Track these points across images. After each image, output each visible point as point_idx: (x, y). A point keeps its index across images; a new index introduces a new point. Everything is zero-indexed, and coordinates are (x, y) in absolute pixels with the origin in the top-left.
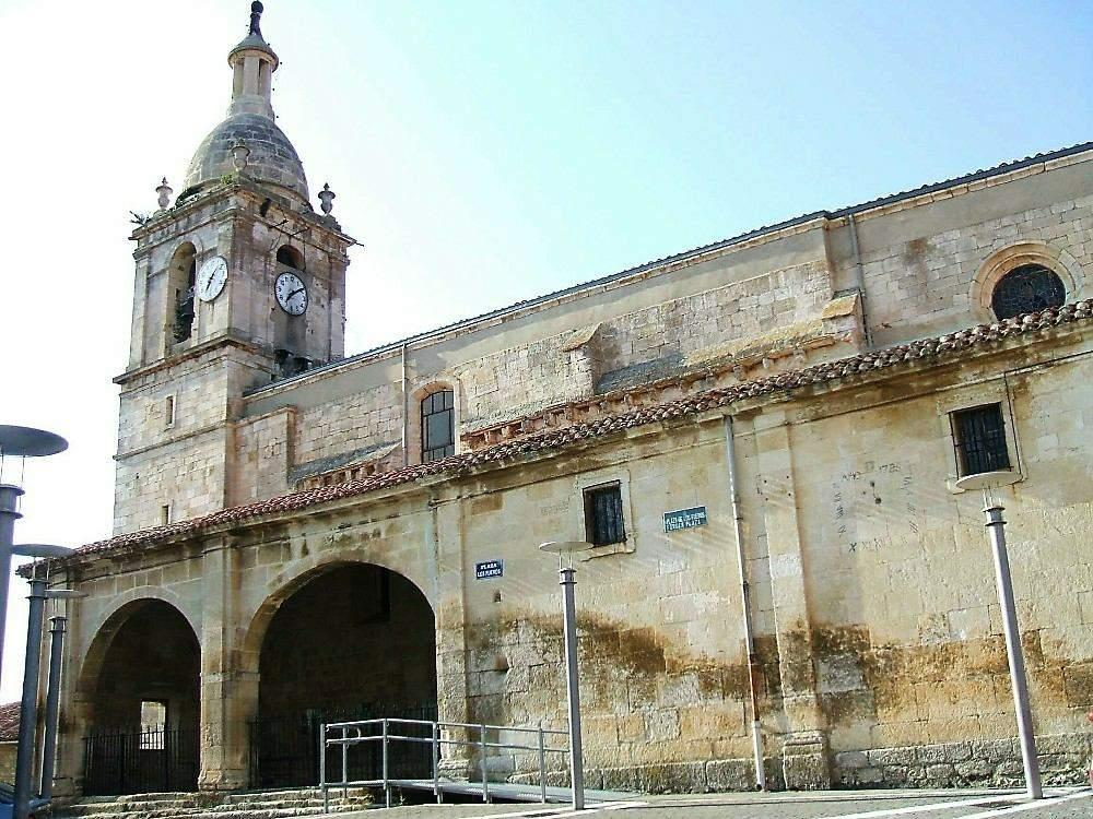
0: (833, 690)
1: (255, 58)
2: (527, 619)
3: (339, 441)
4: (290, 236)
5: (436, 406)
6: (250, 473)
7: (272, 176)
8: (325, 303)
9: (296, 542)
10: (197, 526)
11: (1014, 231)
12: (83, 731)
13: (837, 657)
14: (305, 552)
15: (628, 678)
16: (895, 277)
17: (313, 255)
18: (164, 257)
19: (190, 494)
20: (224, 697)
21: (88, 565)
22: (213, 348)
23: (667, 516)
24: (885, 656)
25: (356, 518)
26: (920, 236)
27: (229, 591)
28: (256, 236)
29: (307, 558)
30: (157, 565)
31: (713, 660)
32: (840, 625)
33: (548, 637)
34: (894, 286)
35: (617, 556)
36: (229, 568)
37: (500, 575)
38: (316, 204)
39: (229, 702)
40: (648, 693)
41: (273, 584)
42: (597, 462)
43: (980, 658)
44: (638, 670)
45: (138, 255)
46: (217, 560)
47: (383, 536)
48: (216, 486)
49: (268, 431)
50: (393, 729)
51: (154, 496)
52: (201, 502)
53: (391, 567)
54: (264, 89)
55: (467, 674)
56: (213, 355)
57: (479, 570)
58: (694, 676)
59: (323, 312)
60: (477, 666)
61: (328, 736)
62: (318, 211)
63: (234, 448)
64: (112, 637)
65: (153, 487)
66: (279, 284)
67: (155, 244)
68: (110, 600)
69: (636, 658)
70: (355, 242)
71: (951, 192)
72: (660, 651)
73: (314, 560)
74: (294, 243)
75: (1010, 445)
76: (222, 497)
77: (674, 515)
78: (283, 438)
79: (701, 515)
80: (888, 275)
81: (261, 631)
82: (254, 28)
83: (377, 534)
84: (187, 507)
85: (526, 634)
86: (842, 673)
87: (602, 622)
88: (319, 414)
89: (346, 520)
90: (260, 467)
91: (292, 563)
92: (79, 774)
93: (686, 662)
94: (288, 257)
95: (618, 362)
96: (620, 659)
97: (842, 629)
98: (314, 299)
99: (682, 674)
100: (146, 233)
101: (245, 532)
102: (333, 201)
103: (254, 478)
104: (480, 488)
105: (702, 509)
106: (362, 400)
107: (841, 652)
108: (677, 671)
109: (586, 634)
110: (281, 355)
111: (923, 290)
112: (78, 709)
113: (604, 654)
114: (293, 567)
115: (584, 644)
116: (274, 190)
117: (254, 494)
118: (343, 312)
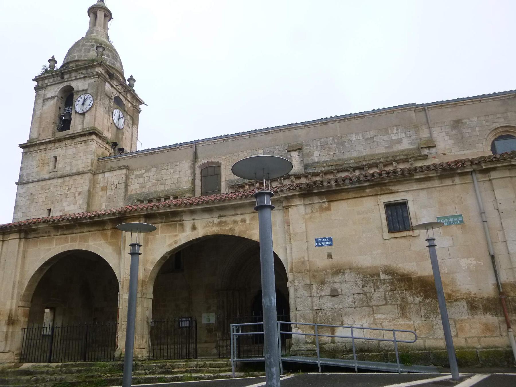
1: (99, 13)
2: (350, 269)
3: (155, 185)
4: (120, 93)
5: (210, 173)
6: (101, 197)
7: (112, 64)
8: (131, 126)
10: (56, 220)
12: (22, 324)
14: (194, 228)
15: (420, 302)
16: (447, 134)
18: (54, 91)
19: (65, 204)
21: (35, 230)
22: (84, 135)
26: (459, 118)
28: (107, 88)
29: (196, 232)
30: (86, 232)
31: (475, 294)
33: (365, 279)
34: (447, 138)
35: (408, 237)
37: (332, 245)
41: (171, 245)
42: (391, 190)
44: (426, 297)
45: (37, 89)
47: (248, 222)
48: (81, 201)
51: (41, 204)
56: (83, 139)
57: (317, 241)
58: (464, 303)
59: (130, 130)
60: (318, 293)
63: (93, 183)
64: (45, 271)
67: (48, 84)
68: (50, 249)
69: (425, 291)
71: (473, 101)
73: (200, 233)
74: (121, 97)
76: (86, 207)
78: (123, 181)
79: (459, 219)
80: (444, 134)
81: (158, 269)
83: (244, 221)
85: (349, 277)
87: (402, 271)
88: (143, 171)
89: (222, 213)
90: (108, 194)
91: (184, 234)
92: (17, 350)
93: (458, 294)
94: (118, 102)
95: (312, 159)
96: (414, 291)
99: (456, 300)
100: (42, 81)
103: (104, 199)
105: (461, 216)
106: (169, 167)
109: (390, 277)
110: (114, 145)
111: (461, 141)
112: (20, 311)
113: (402, 288)
115: (389, 283)
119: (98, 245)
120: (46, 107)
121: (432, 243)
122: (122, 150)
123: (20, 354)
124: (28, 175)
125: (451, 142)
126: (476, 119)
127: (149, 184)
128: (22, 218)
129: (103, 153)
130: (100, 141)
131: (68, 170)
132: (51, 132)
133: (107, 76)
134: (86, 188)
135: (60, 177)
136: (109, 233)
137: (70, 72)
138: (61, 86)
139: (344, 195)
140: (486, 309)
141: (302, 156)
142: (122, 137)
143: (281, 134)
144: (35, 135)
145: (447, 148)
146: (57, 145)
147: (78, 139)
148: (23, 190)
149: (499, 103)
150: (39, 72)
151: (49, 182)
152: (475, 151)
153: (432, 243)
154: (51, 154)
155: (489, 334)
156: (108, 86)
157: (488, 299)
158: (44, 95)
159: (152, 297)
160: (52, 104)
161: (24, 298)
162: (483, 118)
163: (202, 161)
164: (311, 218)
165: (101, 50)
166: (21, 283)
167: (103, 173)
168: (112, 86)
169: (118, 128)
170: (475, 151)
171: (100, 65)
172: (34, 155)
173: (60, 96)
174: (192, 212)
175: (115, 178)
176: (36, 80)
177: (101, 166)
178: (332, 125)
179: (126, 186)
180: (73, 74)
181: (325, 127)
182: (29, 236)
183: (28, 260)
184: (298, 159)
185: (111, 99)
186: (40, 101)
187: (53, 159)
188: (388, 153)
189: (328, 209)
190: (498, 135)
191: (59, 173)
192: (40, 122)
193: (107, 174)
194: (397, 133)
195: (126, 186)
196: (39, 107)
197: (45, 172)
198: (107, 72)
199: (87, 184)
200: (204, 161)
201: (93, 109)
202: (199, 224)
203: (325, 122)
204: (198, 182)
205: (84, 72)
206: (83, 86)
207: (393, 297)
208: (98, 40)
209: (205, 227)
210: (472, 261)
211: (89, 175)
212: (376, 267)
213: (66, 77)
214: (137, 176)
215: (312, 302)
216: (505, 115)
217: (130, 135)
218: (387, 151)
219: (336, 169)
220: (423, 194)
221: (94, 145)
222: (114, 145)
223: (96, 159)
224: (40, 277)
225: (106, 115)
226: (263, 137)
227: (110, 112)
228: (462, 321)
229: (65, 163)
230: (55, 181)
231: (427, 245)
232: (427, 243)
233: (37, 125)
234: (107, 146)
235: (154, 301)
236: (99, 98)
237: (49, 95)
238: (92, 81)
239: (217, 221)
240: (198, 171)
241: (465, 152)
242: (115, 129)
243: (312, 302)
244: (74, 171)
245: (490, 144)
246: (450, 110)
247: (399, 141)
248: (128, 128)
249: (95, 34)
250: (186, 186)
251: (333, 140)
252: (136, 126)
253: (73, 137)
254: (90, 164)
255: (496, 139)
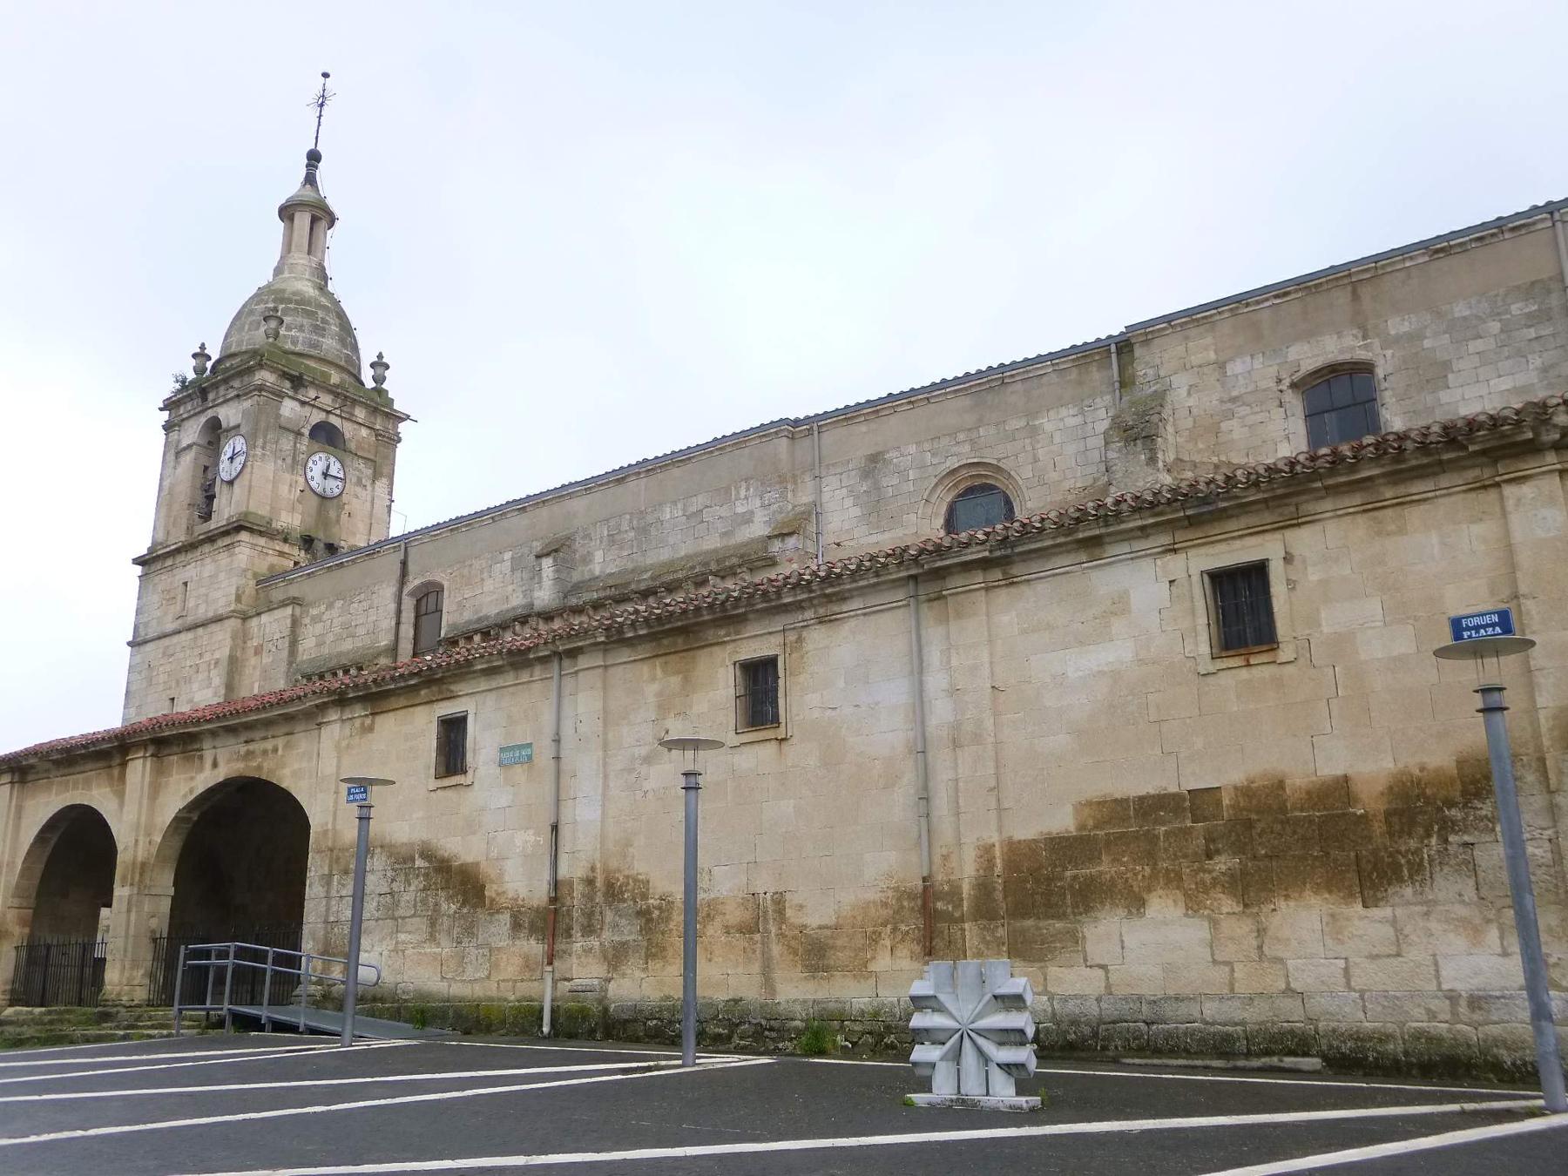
0: (616, 938)
1: (308, 215)
3: (340, 639)
4: (328, 412)
5: (428, 599)
6: (254, 668)
8: (368, 484)
9: (208, 756)
11: (967, 448)
13: (622, 906)
14: (215, 765)
17: (355, 433)
18: (192, 432)
19: (195, 686)
20: (129, 911)
21: (32, 767)
22: (226, 533)
23: (502, 750)
24: (660, 908)
25: (257, 735)
27: (145, 801)
29: (216, 772)
32: (626, 873)
34: (849, 502)
36: (147, 779)
38: (367, 376)
39: (133, 917)
40: (470, 931)
41: (185, 796)
43: (735, 915)
44: (464, 904)
45: (168, 427)
46: (139, 769)
48: (218, 679)
49: (273, 625)
50: (240, 953)
51: (161, 688)
52: (202, 694)
53: (283, 786)
54: (313, 245)
55: (328, 897)
56: (227, 540)
58: (505, 918)
61: (187, 957)
62: (369, 384)
63: (241, 638)
64: (53, 843)
65: (162, 678)
66: (310, 464)
69: (465, 893)
70: (408, 417)
72: (483, 887)
73: (221, 775)
75: (781, 702)
76: (223, 692)
77: (512, 748)
78: (287, 632)
81: (177, 843)
82: (310, 180)
83: (275, 750)
84: (191, 701)
86: (623, 922)
88: (323, 608)
94: (326, 436)
97: (627, 877)
98: (354, 480)
99: (498, 912)
101: (163, 740)
102: (387, 373)
104: (359, 711)
105: (530, 745)
107: (624, 901)
108: (494, 909)
110: (308, 542)
111: (875, 509)
114: (205, 778)
116: (312, 364)
117: (253, 685)
118: (390, 493)
119: (97, 795)
120: (179, 470)
121: (1494, 698)
122: (332, 549)
123: (13, 991)
124: (146, 624)
125: (857, 511)
126: (912, 449)
127: (330, 637)
128: (154, 709)
129: (272, 567)
130: (262, 541)
131: (203, 612)
132: (184, 526)
133: (288, 384)
134: (225, 652)
135: (189, 629)
136: (116, 772)
137: (215, 386)
138: (203, 419)
139: (394, 702)
140: (533, 930)
141: (563, 567)
142: (339, 516)
143: (544, 512)
144: (161, 537)
145: (848, 528)
146: (190, 556)
147: (220, 543)
148: (138, 658)
149: (966, 402)
150: (169, 388)
151: (175, 639)
152: (899, 532)
153: (1494, 698)
154: (181, 575)
155: (527, 975)
156: (289, 408)
157: (537, 910)
158: (179, 441)
159: (172, 891)
160: (188, 458)
161: (19, 892)
162: (927, 446)
163: (414, 582)
164: (348, 746)
165: (273, 324)
166: (11, 864)
167: (259, 614)
168: (303, 403)
169: (323, 498)
170: (899, 532)
171: (261, 366)
172: (157, 579)
173: (203, 442)
174: (214, 734)
175: (275, 625)
176: (169, 405)
177: (266, 592)
178: (632, 484)
179: (294, 643)
180: (222, 390)
181: (620, 489)
182: (30, 777)
183: (25, 822)
184: (551, 575)
185: (299, 434)
186: (171, 457)
187: (182, 588)
188: (727, 548)
189: (371, 729)
190: (962, 486)
191: (190, 620)
192: (170, 506)
193: (265, 618)
194: (746, 498)
195: (294, 643)
196: (169, 470)
197: (170, 617)
198: (285, 375)
199: (228, 642)
200: (417, 582)
201: (248, 470)
202: (223, 756)
203: (620, 477)
204: (407, 631)
205: (236, 383)
206: (281, 387)
207: (424, 902)
208: (284, 291)
209: (229, 761)
210: (530, 836)
211: (233, 623)
212: (412, 844)
213: (211, 396)
214: (317, 619)
215: (328, 910)
216: (974, 435)
217: (368, 504)
218: (725, 543)
219: (606, 598)
220: (491, 699)
221: (246, 554)
222: (308, 542)
223: (252, 583)
224: (47, 854)
225: (287, 476)
226: (518, 522)
227: (298, 464)
228: (499, 949)
229: (198, 597)
230: (183, 636)
231: (1480, 706)
232: (1478, 701)
233: (163, 511)
234: (286, 548)
235: (174, 899)
236: (260, 442)
237: (184, 444)
238: (247, 404)
239: (243, 749)
240: (408, 604)
241: (880, 537)
242: (315, 501)
243: (328, 910)
244: (210, 614)
245: (944, 509)
246: (863, 428)
247: (747, 519)
248: (359, 489)
249: (286, 275)
250: (385, 641)
251: (631, 521)
252: (384, 480)
253: (211, 539)
254: (233, 597)
255: (960, 495)
